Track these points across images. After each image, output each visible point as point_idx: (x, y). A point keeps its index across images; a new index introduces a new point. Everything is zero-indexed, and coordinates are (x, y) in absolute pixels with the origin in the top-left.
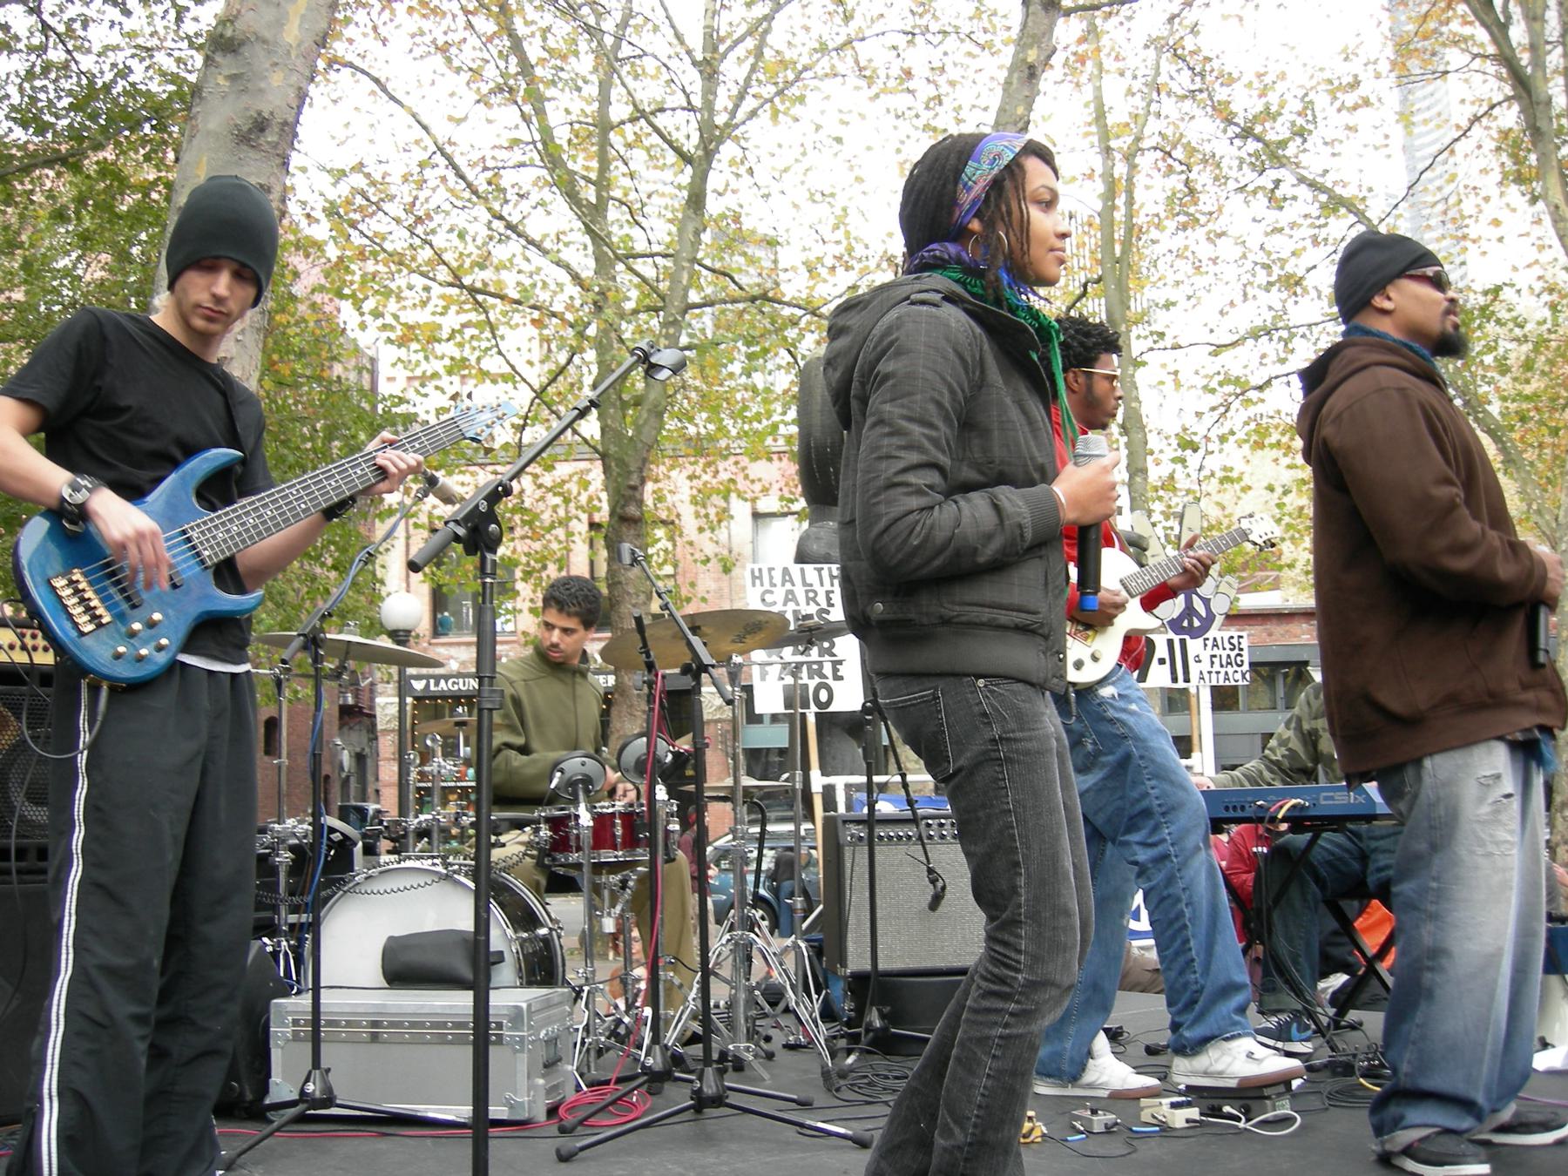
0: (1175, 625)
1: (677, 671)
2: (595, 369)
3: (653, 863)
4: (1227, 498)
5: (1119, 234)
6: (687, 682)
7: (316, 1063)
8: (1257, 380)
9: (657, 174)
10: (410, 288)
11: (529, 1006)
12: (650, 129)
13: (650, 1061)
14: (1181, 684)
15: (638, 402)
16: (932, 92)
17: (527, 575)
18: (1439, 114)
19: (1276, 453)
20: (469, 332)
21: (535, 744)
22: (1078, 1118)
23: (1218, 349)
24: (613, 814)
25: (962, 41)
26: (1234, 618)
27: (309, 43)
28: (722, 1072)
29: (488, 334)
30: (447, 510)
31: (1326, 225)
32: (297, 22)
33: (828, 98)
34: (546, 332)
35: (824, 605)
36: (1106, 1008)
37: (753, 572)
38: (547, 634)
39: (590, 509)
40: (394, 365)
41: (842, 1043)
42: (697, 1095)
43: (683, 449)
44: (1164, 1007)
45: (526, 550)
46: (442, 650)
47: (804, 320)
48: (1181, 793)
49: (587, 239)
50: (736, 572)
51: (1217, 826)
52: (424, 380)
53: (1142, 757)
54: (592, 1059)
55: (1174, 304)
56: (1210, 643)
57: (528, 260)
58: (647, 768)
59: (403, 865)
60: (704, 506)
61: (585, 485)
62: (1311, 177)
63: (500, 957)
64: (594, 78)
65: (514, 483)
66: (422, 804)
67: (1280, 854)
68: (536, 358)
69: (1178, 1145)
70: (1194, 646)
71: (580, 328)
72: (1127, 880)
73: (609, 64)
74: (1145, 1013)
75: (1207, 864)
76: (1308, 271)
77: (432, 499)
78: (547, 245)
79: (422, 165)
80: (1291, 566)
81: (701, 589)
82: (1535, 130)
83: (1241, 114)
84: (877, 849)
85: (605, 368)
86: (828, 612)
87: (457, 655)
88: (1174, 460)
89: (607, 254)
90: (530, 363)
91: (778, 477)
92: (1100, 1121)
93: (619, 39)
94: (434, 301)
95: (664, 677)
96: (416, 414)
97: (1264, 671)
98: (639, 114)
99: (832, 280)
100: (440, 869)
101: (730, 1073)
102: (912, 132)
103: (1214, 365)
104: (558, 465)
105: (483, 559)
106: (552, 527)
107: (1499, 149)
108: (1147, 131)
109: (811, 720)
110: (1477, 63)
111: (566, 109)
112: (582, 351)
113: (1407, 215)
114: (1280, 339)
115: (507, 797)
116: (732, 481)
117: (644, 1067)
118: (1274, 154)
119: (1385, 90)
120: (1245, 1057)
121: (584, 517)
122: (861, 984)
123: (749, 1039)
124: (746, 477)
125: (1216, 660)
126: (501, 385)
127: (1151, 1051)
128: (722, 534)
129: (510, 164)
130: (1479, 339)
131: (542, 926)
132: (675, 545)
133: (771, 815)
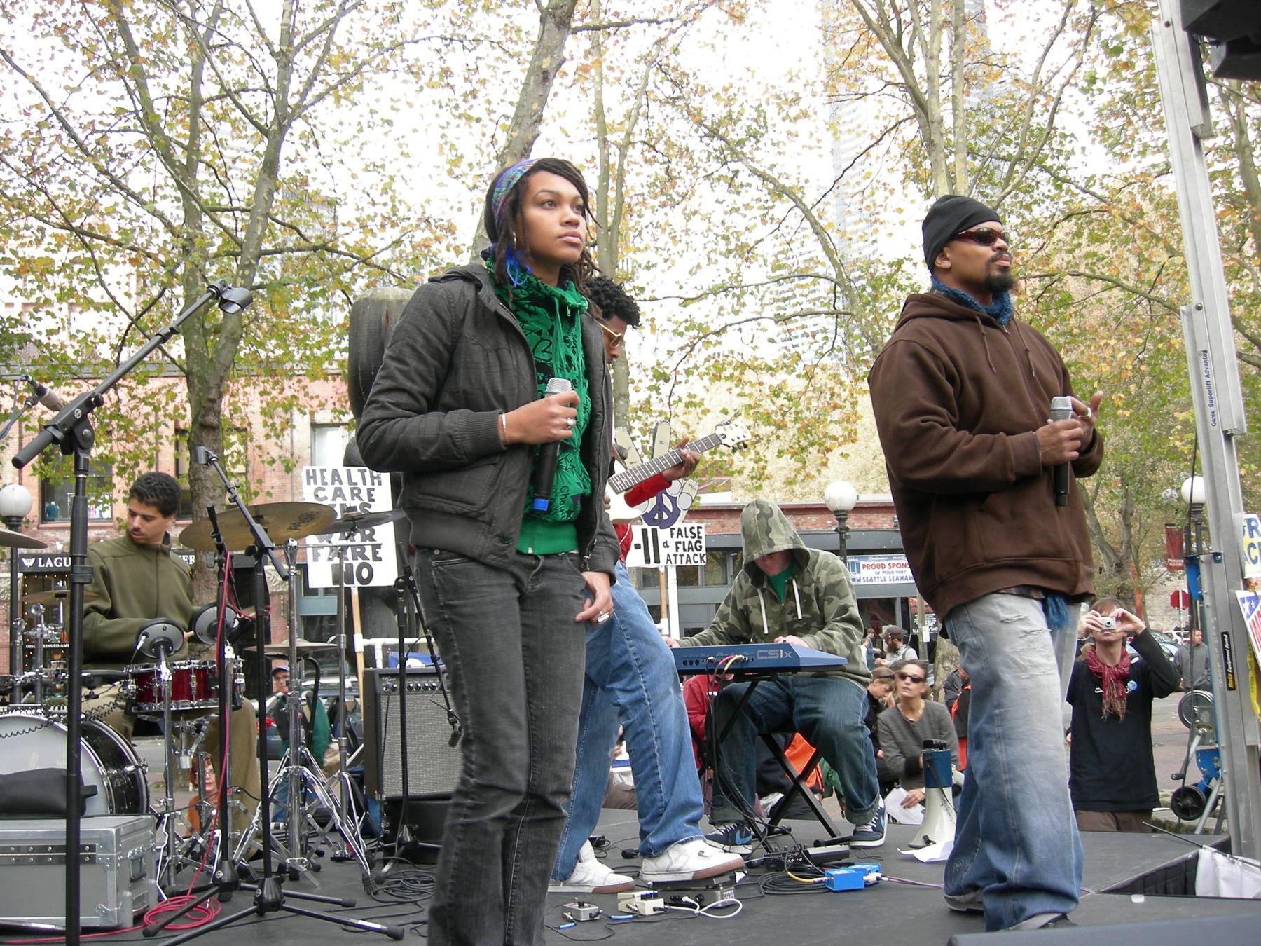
0: (648, 518)
1: (243, 552)
2: (182, 301)
3: (222, 711)
4: (691, 418)
5: (611, 208)
6: (251, 562)
8: (715, 327)
9: (241, 143)
10: (27, 228)
11: (118, 831)
12: (233, 106)
13: (220, 874)
14: (652, 565)
15: (217, 330)
16: (469, 87)
17: (122, 471)
18: (859, 126)
19: (729, 384)
20: (77, 267)
21: (121, 609)
22: (568, 910)
23: (686, 302)
24: (189, 670)
25: (493, 48)
26: (694, 513)
28: (279, 882)
29: (92, 268)
30: (50, 415)
31: (772, 207)
33: (380, 88)
34: (142, 269)
35: (366, 500)
36: (592, 822)
37: (308, 472)
39: (176, 417)
40: (12, 292)
41: (380, 855)
42: (259, 901)
43: (256, 370)
44: (637, 821)
45: (121, 449)
46: (49, 534)
47: (356, 267)
48: (653, 649)
49: (179, 194)
50: (296, 471)
51: (683, 673)
52: (37, 306)
53: (622, 622)
54: (172, 874)
56: (675, 532)
57: (129, 210)
58: (220, 632)
59: (10, 714)
60: (271, 417)
61: (172, 397)
62: (761, 170)
63: (93, 791)
64: (187, 60)
65: (104, 396)
66: (29, 663)
67: (726, 699)
68: (133, 290)
69: (647, 929)
70: (663, 534)
71: (170, 268)
72: (612, 721)
73: (201, 48)
74: (621, 825)
75: (672, 710)
76: (757, 243)
77: (40, 406)
78: (146, 197)
79: (39, 125)
80: (740, 472)
81: (267, 485)
82: (930, 144)
83: (709, 117)
84: (407, 697)
85: (189, 299)
86: (370, 506)
87: (58, 539)
88: (650, 388)
90: (128, 295)
91: (331, 393)
92: (586, 911)
93: (210, 31)
94: (47, 239)
95: (232, 557)
96: (30, 335)
97: (718, 555)
98: (226, 93)
99: (380, 235)
100: (43, 718)
101: (287, 883)
102: (451, 119)
103: (682, 314)
104: (150, 380)
105: (77, 459)
106: (144, 431)
107: (903, 155)
108: (636, 130)
109: (355, 593)
110: (889, 89)
111: (165, 85)
112: (172, 286)
113: (833, 202)
114: (734, 295)
115: (102, 656)
116: (294, 397)
117: (215, 879)
118: (733, 150)
119: (818, 104)
120: (697, 855)
121: (171, 424)
122: (393, 806)
123: (303, 853)
124: (306, 394)
125: (681, 546)
126: (104, 313)
127: (627, 855)
128: (286, 441)
129: (116, 128)
130: (885, 300)
131: (129, 764)
132: (246, 449)
133: (324, 670)
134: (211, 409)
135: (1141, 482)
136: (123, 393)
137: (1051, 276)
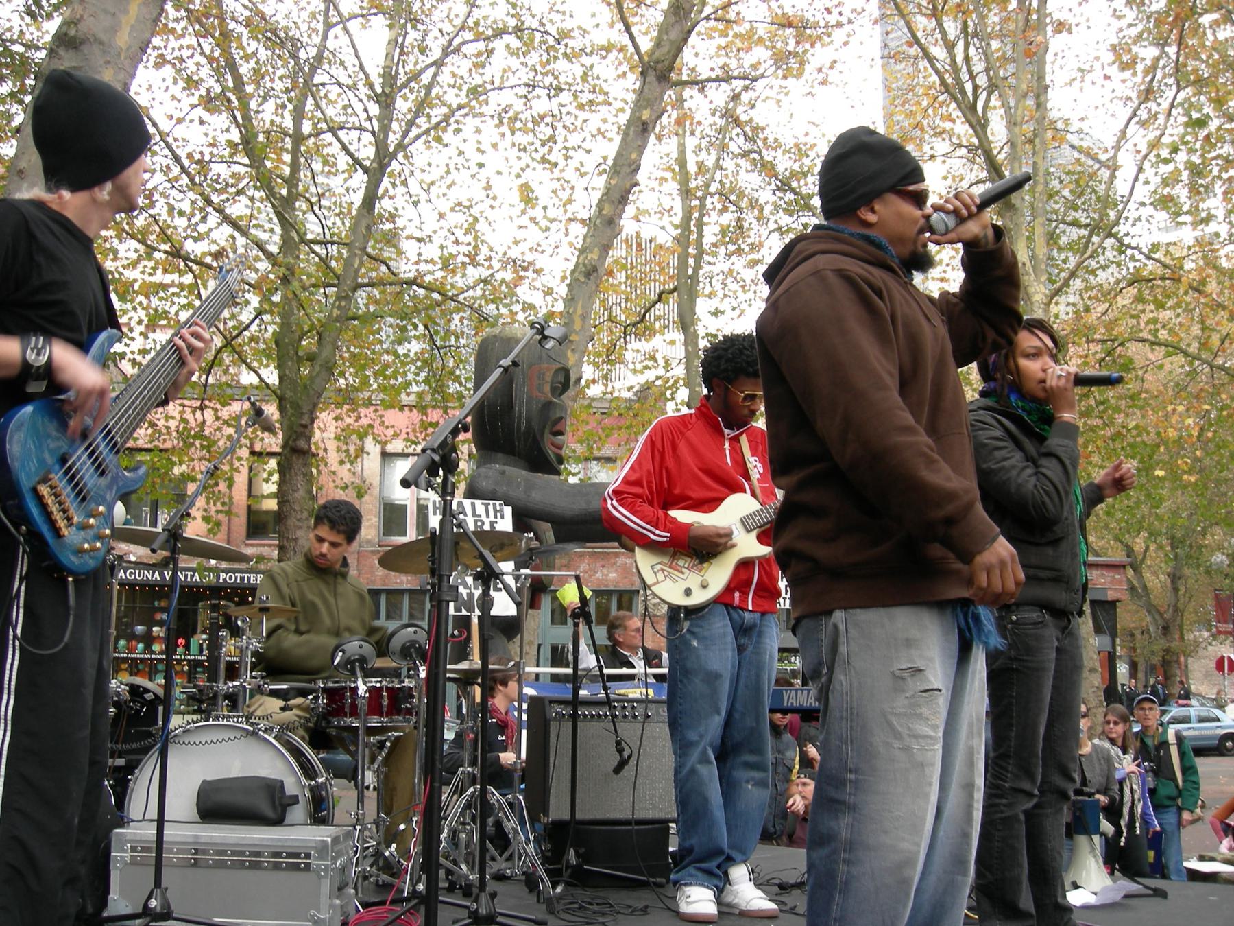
7: (158, 883)
15: (311, 358)
24: (381, 688)
27: (135, 48)
32: (128, 29)
38: (317, 545)
55: (722, 313)
60: (347, 444)
63: (295, 800)
89: (293, 237)
102: (529, 161)
109: (475, 620)
116: (371, 426)
122: (558, 826)
124: (382, 423)
134: (302, 434)
135: (1191, 546)
136: (209, 414)
137: (1113, 341)
